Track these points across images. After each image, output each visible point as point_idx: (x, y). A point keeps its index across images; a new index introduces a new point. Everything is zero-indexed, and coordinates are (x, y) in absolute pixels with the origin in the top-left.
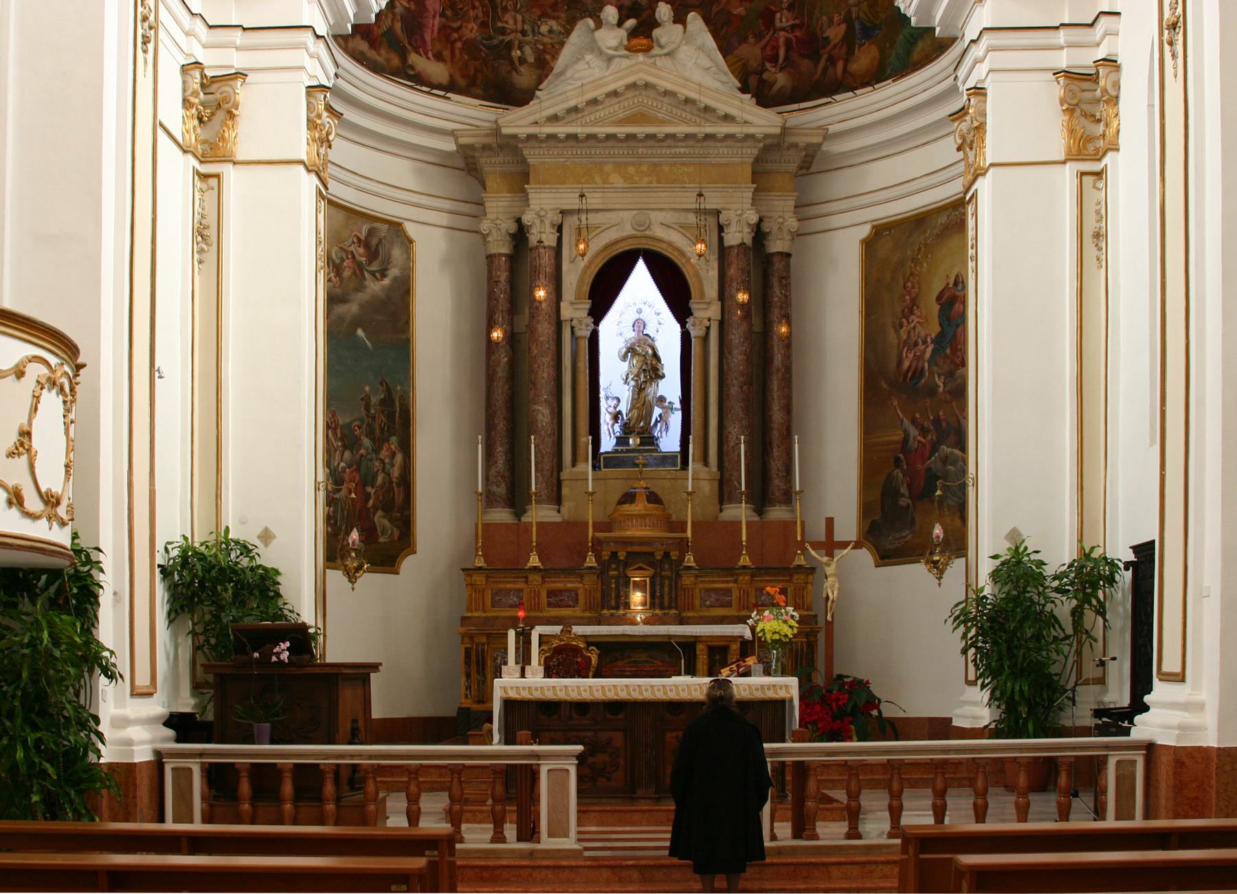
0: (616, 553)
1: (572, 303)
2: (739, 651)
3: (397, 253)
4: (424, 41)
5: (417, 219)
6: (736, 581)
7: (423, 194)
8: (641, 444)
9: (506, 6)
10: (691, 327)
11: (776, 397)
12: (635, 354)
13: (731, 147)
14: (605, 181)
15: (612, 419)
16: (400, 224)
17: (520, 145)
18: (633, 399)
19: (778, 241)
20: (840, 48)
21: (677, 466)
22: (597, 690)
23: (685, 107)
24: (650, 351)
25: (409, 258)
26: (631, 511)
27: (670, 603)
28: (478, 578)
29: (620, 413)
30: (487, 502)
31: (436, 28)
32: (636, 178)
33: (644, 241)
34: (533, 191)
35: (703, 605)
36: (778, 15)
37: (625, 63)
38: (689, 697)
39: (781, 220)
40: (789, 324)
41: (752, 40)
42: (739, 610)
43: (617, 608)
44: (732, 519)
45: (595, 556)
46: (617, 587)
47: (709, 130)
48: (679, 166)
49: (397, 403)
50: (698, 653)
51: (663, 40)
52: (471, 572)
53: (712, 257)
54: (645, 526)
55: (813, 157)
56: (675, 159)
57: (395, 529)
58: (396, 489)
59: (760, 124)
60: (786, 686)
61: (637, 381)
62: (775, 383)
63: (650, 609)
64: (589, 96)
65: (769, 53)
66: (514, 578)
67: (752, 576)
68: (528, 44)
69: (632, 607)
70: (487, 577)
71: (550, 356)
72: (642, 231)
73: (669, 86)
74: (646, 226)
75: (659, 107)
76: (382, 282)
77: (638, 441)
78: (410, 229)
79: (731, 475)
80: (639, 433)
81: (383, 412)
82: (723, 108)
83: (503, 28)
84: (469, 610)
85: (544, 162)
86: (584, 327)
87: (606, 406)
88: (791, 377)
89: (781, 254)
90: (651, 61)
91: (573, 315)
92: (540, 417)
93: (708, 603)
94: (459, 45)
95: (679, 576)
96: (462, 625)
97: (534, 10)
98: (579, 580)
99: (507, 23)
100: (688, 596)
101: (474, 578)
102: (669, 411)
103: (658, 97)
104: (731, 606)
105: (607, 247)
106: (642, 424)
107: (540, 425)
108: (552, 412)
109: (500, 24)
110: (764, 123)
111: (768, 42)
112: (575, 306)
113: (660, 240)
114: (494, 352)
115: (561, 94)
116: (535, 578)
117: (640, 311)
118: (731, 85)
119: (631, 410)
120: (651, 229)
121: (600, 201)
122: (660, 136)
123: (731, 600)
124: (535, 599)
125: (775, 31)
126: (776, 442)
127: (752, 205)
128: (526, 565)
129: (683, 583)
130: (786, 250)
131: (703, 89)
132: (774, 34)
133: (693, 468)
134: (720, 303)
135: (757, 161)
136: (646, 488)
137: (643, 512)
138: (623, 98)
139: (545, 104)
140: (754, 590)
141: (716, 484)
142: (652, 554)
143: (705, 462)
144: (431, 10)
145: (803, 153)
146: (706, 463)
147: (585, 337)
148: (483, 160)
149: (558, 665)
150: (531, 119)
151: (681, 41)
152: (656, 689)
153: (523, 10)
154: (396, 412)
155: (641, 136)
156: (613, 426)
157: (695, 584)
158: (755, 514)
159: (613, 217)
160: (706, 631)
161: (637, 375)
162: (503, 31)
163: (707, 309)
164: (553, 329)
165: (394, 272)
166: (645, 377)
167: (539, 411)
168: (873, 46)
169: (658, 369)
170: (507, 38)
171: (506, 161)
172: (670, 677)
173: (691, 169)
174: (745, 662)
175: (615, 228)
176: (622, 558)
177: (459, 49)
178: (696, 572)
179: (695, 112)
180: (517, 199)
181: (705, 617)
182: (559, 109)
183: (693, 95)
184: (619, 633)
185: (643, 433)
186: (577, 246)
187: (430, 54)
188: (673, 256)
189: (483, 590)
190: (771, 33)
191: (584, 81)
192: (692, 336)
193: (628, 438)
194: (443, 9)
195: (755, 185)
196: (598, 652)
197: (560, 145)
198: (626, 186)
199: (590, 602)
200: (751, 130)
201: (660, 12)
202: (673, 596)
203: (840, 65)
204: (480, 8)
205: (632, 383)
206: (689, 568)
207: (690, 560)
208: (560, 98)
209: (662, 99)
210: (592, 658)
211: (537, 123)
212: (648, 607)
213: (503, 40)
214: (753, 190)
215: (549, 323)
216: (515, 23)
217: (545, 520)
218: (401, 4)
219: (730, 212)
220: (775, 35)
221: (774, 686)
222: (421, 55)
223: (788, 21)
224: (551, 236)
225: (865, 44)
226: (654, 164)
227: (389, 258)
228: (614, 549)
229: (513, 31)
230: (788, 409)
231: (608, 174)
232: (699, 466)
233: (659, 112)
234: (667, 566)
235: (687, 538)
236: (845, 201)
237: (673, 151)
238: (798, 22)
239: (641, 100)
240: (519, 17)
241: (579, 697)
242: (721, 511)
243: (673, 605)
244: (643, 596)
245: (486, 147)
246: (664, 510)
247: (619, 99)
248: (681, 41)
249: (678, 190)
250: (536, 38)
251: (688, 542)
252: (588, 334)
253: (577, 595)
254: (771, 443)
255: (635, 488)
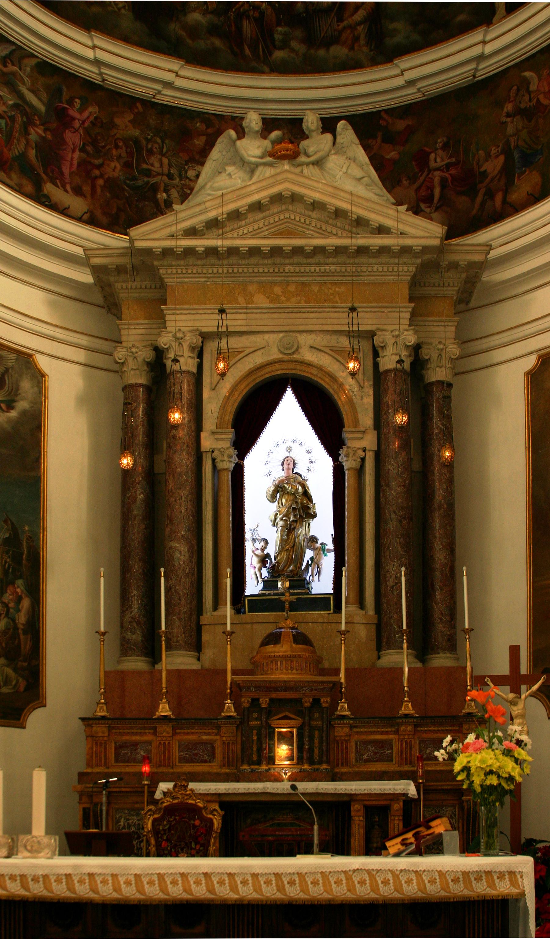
0: (258, 700)
1: (213, 433)
2: (402, 811)
3: (26, 385)
4: (62, 174)
5: (49, 352)
6: (397, 732)
7: (56, 326)
8: (291, 587)
9: (151, 149)
10: (345, 459)
11: (438, 535)
12: (285, 493)
13: (386, 264)
14: (250, 301)
15: (259, 562)
16: (31, 356)
17: (156, 263)
18: (282, 540)
19: (438, 369)
20: (499, 180)
21: (330, 610)
22: (151, 883)
23: (335, 222)
24: (300, 489)
25: (40, 392)
26: (275, 652)
27: (321, 756)
28: (99, 729)
29: (268, 555)
30: (122, 650)
31: (75, 162)
32: (283, 299)
33: (293, 366)
34: (170, 312)
35: (359, 759)
36: (432, 156)
37: (269, 172)
38: (326, 896)
39: (441, 346)
40: (452, 449)
41: (405, 183)
42: (400, 765)
43: (259, 763)
44: (391, 665)
45: (234, 704)
46: (259, 739)
47: (361, 242)
48: (330, 286)
49: (25, 544)
50: (353, 814)
51: (311, 150)
52: (91, 722)
53: (366, 384)
54: (292, 669)
55: (474, 284)
56: (326, 278)
57: (21, 680)
58: (22, 637)
59: (417, 235)
60: (512, 873)
61: (286, 521)
62: (437, 520)
63: (298, 764)
64: (231, 207)
65: (423, 194)
66: (140, 729)
67: (416, 726)
68: (174, 187)
69: (277, 762)
70: (110, 729)
71: (188, 488)
72: (290, 354)
73: (317, 196)
74: (293, 350)
75: (308, 222)
76: (8, 414)
77: (287, 584)
78: (43, 362)
79: (390, 618)
80: (288, 576)
81: (7, 552)
82: (376, 219)
83: (149, 170)
84: (89, 765)
85: (182, 282)
86: (226, 458)
87: (252, 548)
88: (454, 515)
89: (441, 383)
90: (298, 170)
91: (214, 446)
92: (177, 555)
93: (365, 757)
94: (100, 182)
95: (330, 726)
96: (80, 781)
97: (181, 154)
98: (216, 731)
99: (152, 165)
100: (342, 750)
101: (94, 729)
102: (322, 552)
103: (306, 212)
104: (392, 761)
105: (251, 373)
106: (291, 568)
107: (177, 564)
108: (190, 550)
109: (144, 166)
110: (422, 234)
111: (423, 183)
112: (216, 436)
113: (309, 365)
114: (129, 489)
115: (199, 204)
116: (166, 730)
117: (289, 450)
118: (385, 198)
119: (279, 553)
120: (299, 353)
121: (244, 322)
122: (308, 249)
123: (392, 753)
124: (164, 752)
125: (429, 171)
126: (438, 585)
127: (410, 325)
128: (155, 715)
129: (336, 734)
130: (448, 379)
131: (355, 199)
132: (428, 175)
133: (346, 611)
134: (376, 432)
135: (414, 283)
136: (293, 628)
137: (289, 653)
138: (267, 213)
139: (182, 215)
140: (418, 742)
141: (373, 629)
142: (299, 701)
143: (361, 604)
144: (70, 143)
145: (464, 276)
146: (361, 605)
147: (227, 470)
148: (118, 286)
149: (170, 829)
150: (167, 231)
151: (330, 151)
152: (262, 880)
153: (169, 153)
154: (22, 554)
155: (287, 249)
156: (260, 569)
157: (350, 735)
158: (416, 660)
159: (258, 340)
160: (363, 787)
161: (287, 515)
162: (148, 173)
163: (362, 438)
164: (191, 459)
165: (22, 405)
166: (295, 516)
167: (175, 548)
168: (534, 172)
169: (309, 508)
170: (153, 180)
171: (143, 287)
172: (294, 855)
173: (343, 289)
174: (429, 828)
175: (259, 353)
176: (264, 706)
177: (101, 186)
178: (351, 722)
179: (347, 227)
180: (154, 326)
181: (362, 772)
182: (197, 221)
183: (345, 206)
184: (259, 791)
185: (292, 577)
186: (216, 365)
187: (68, 187)
188: (325, 383)
189: (105, 743)
190: (426, 173)
191: (225, 191)
192: (345, 468)
193: (277, 581)
194: (84, 144)
195: (413, 305)
196: (222, 813)
197: (199, 262)
198: (272, 305)
199: (228, 756)
200: (408, 242)
201: (307, 122)
202: (324, 748)
203: (499, 198)
204: (124, 148)
205: (281, 523)
206: (343, 717)
207: (343, 708)
208: (197, 209)
209: (310, 213)
210: (215, 821)
211: (173, 236)
212: (295, 761)
213: (148, 182)
214: (410, 310)
215: (188, 453)
216: (161, 166)
217: (182, 667)
218: (37, 132)
219: (387, 333)
220: (430, 176)
221: (489, 873)
222: (57, 186)
223: (442, 160)
224: (190, 361)
225: (525, 171)
226: (303, 284)
227: (18, 389)
228: (256, 696)
229: (158, 174)
230: (451, 548)
231: (253, 295)
232: (354, 609)
233: (308, 229)
234: (317, 715)
235: (341, 683)
236: (509, 333)
237: (322, 269)
238: (453, 160)
239: (287, 216)
240: (165, 161)
241: (115, 895)
242: (379, 658)
243: (324, 758)
244: (290, 749)
245: (120, 270)
246: (314, 652)
247: (265, 214)
248: (330, 151)
249: (328, 310)
250: (182, 182)
251: (342, 688)
252: (232, 466)
253: (213, 748)
254: (433, 585)
255: (280, 628)
